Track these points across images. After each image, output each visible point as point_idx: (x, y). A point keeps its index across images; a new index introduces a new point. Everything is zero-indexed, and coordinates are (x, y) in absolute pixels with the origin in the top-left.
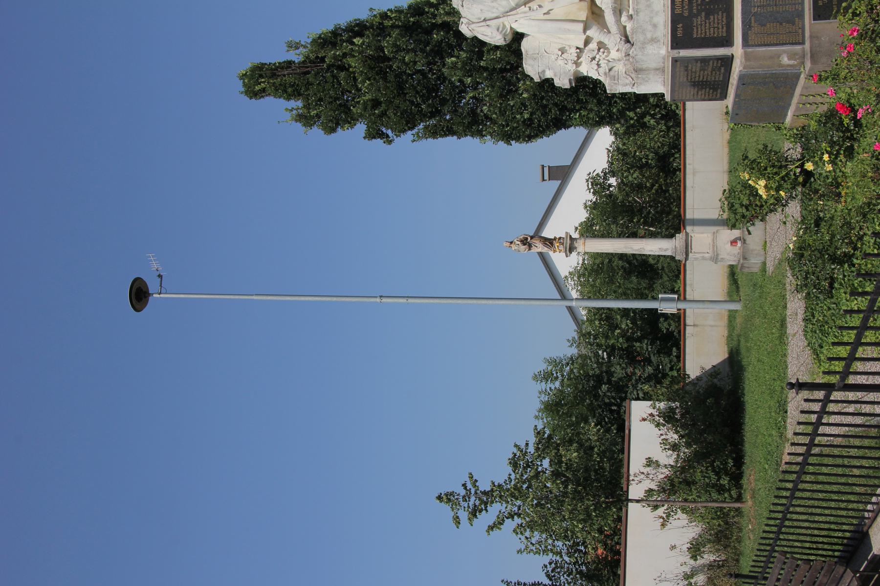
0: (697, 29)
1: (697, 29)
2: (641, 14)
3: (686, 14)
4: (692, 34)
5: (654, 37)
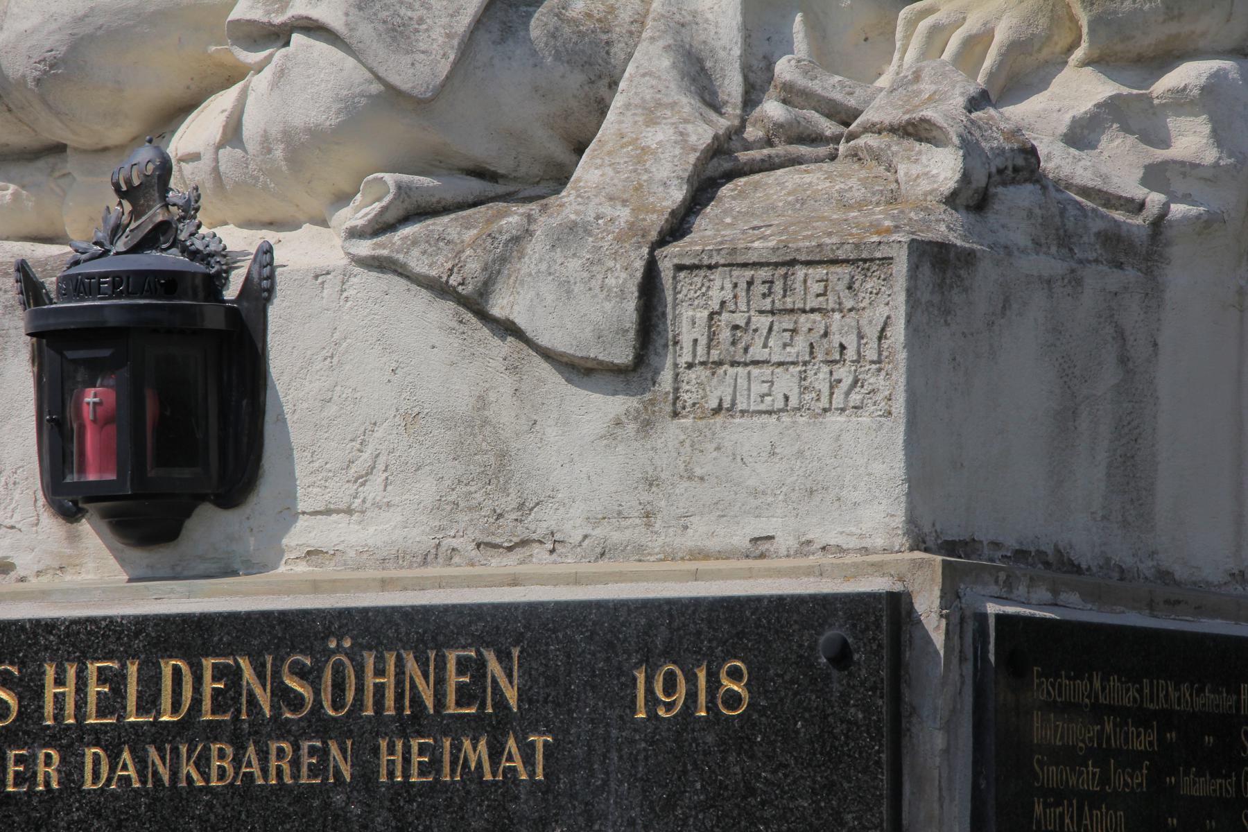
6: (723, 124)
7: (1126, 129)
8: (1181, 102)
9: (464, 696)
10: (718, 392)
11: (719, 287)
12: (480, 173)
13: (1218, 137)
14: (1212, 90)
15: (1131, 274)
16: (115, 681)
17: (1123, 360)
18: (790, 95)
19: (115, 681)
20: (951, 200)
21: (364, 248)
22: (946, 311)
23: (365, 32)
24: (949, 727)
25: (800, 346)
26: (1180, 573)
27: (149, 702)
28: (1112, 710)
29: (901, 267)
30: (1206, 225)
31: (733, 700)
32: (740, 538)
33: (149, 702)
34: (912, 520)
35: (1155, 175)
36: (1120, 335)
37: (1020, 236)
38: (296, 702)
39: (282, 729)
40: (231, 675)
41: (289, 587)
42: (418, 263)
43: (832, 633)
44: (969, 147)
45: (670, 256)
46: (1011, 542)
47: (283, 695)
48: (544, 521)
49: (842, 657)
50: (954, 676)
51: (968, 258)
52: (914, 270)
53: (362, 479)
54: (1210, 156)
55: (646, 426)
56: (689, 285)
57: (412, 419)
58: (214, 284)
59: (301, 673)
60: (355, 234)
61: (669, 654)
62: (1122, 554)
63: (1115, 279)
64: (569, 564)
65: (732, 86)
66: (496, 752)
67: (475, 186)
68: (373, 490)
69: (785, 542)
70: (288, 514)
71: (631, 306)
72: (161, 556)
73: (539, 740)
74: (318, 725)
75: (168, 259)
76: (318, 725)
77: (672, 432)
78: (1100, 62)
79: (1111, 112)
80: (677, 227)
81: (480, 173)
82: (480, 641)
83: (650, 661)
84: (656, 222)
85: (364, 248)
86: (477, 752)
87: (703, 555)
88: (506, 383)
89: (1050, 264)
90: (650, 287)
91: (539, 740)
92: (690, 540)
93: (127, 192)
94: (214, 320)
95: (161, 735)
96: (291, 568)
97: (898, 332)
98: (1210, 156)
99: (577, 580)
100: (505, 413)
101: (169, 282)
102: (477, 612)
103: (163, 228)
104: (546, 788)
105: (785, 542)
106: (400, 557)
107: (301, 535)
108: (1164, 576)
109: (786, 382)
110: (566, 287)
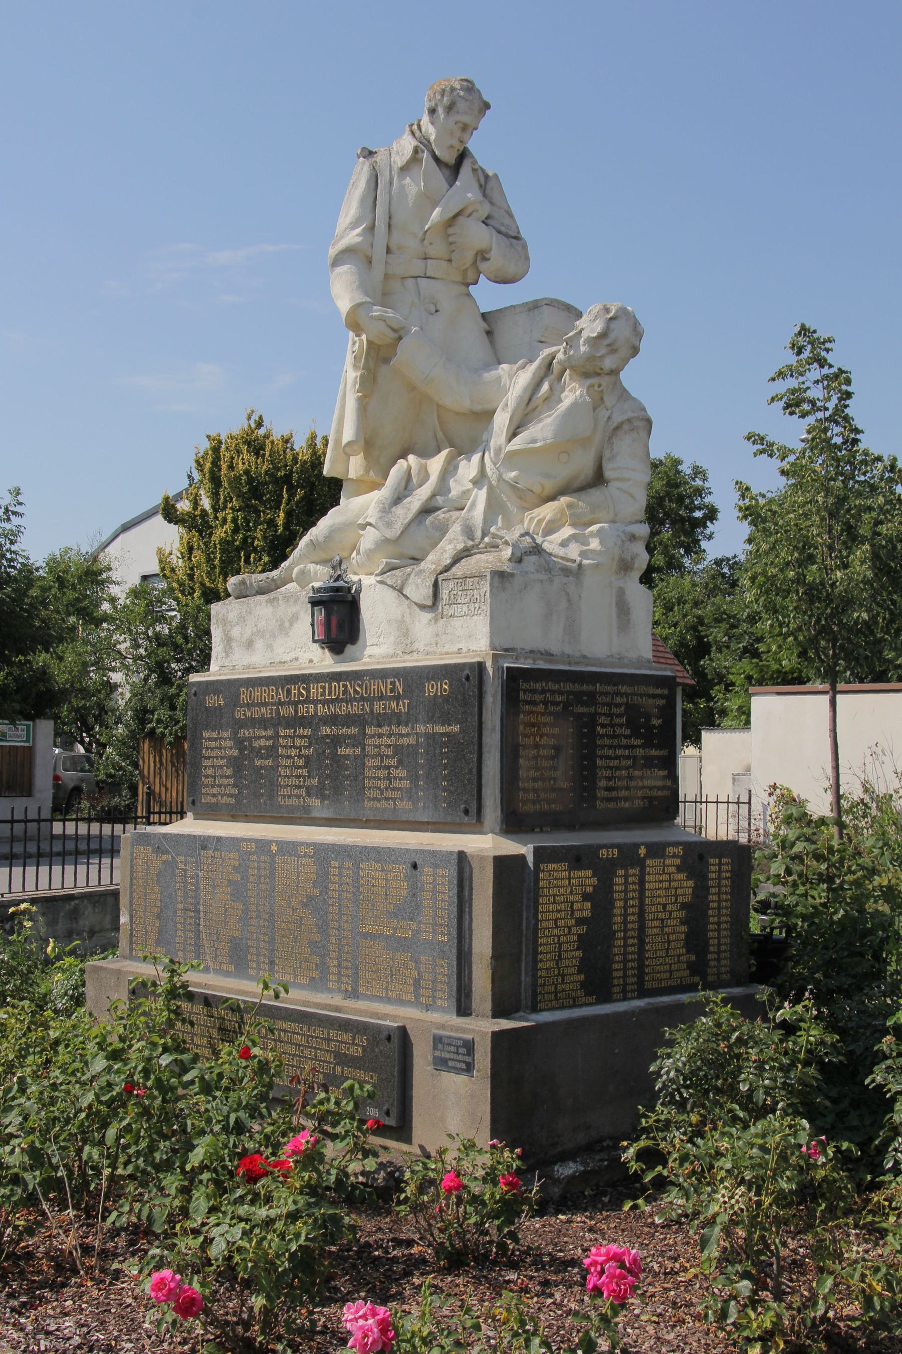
0: (215, 740)
1: (215, 740)
2: (270, 609)
3: (239, 714)
4: (207, 727)
5: (234, 644)
6: (470, 543)
7: (577, 541)
8: (592, 534)
9: (392, 691)
10: (451, 612)
11: (451, 584)
12: (413, 559)
13: (601, 543)
14: (600, 531)
15: (571, 578)
16: (323, 688)
17: (569, 601)
18: (495, 536)
19: (323, 688)
20: (510, 560)
21: (379, 578)
22: (504, 589)
23: (380, 524)
24: (494, 696)
25: (467, 600)
26: (589, 655)
27: (330, 694)
28: (549, 691)
29: (488, 577)
30: (596, 566)
31: (445, 690)
32: (455, 649)
33: (330, 694)
34: (491, 643)
35: (583, 554)
36: (568, 594)
37: (532, 569)
38: (358, 693)
39: (355, 700)
40: (345, 686)
41: (365, 664)
42: (389, 582)
43: (467, 672)
44: (515, 546)
45: (441, 577)
46: (528, 648)
47: (355, 691)
48: (416, 646)
49: (468, 678)
50: (496, 682)
51: (512, 575)
52: (492, 578)
53: (379, 637)
54: (599, 548)
55: (436, 621)
56: (445, 584)
57: (389, 621)
58: (349, 589)
59: (359, 686)
60: (377, 575)
61: (433, 679)
62: (568, 650)
63: (565, 580)
64: (421, 657)
65: (479, 534)
66: (398, 705)
67: (412, 561)
68: (381, 639)
69: (464, 650)
70: (365, 646)
71: (430, 591)
72: (341, 656)
73: (406, 701)
74: (363, 699)
75: (340, 583)
76: (363, 699)
77: (441, 622)
78: (574, 525)
79: (573, 537)
80: (447, 569)
81: (413, 559)
82: (395, 677)
83: (428, 680)
84: (440, 568)
85: (379, 578)
86: (394, 705)
87: (447, 653)
88: (408, 611)
89: (543, 576)
90: (436, 585)
91: (406, 701)
92: (445, 650)
93: (334, 568)
94: (350, 598)
95: (332, 701)
96: (366, 660)
97: (488, 594)
98: (599, 548)
99: (417, 661)
100: (408, 619)
101: (338, 589)
102: (394, 669)
103: (339, 576)
104: (408, 713)
105: (464, 650)
106: (387, 656)
107: (368, 651)
108: (584, 657)
109: (465, 608)
110: (417, 585)
